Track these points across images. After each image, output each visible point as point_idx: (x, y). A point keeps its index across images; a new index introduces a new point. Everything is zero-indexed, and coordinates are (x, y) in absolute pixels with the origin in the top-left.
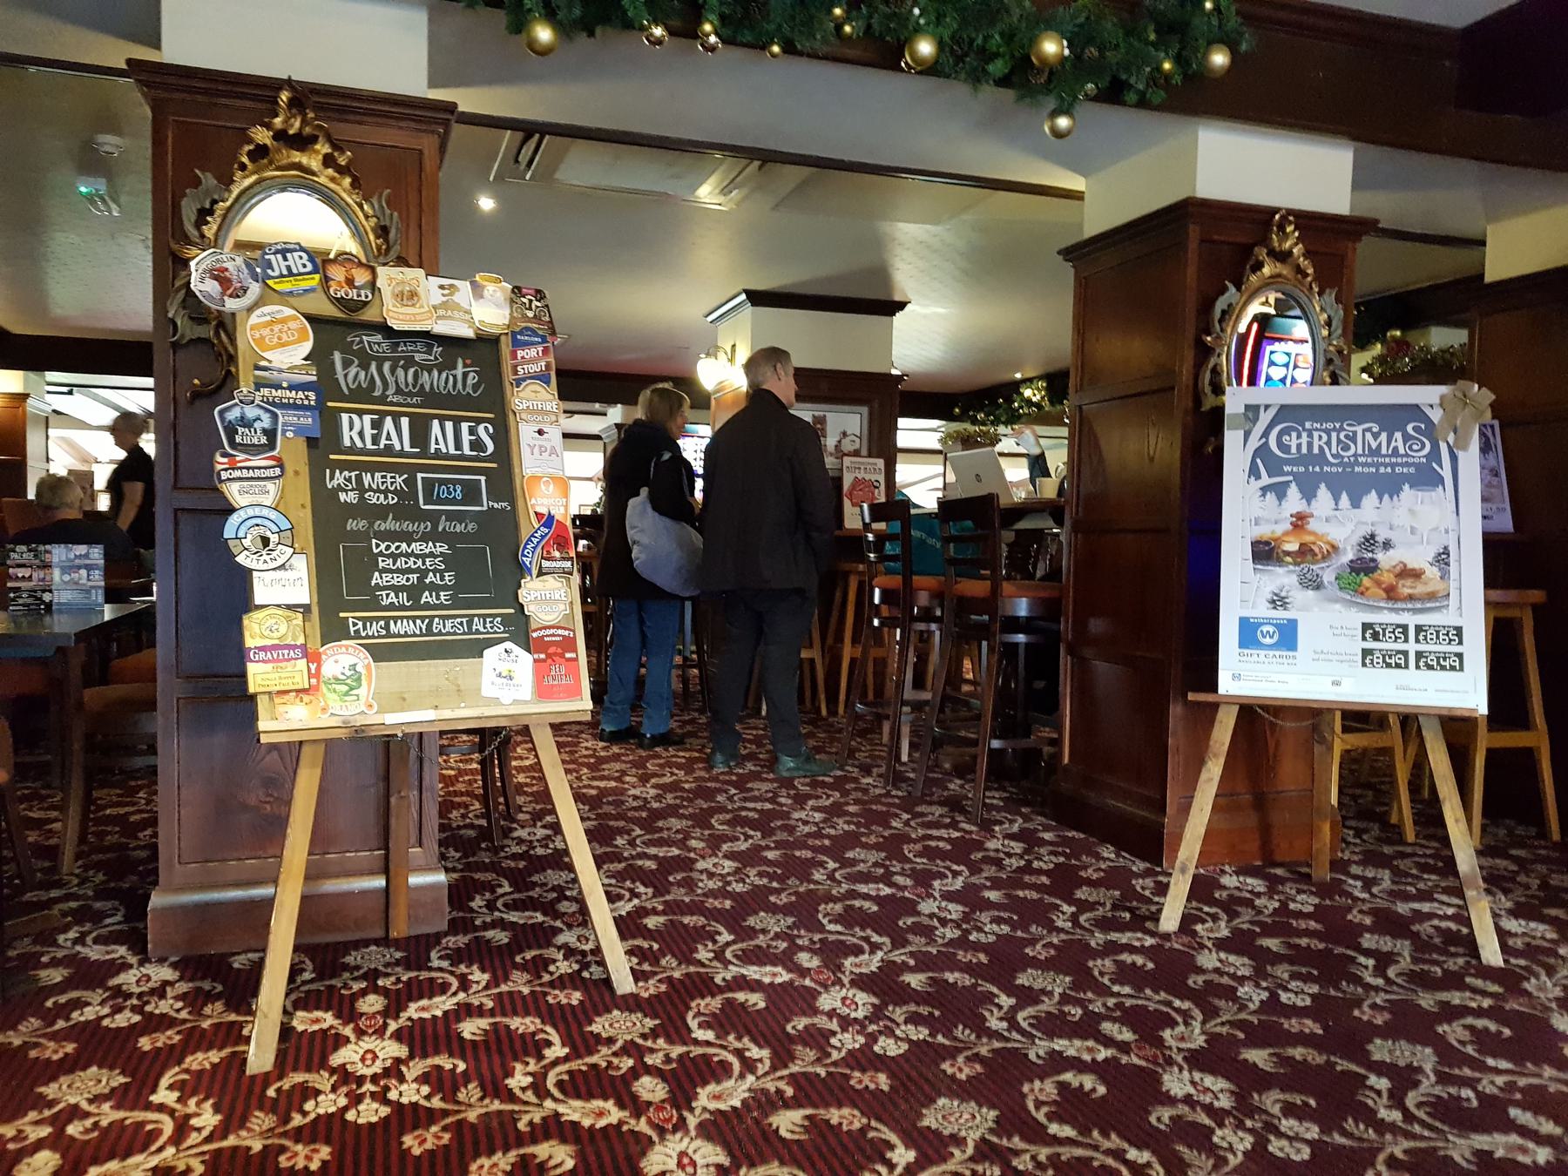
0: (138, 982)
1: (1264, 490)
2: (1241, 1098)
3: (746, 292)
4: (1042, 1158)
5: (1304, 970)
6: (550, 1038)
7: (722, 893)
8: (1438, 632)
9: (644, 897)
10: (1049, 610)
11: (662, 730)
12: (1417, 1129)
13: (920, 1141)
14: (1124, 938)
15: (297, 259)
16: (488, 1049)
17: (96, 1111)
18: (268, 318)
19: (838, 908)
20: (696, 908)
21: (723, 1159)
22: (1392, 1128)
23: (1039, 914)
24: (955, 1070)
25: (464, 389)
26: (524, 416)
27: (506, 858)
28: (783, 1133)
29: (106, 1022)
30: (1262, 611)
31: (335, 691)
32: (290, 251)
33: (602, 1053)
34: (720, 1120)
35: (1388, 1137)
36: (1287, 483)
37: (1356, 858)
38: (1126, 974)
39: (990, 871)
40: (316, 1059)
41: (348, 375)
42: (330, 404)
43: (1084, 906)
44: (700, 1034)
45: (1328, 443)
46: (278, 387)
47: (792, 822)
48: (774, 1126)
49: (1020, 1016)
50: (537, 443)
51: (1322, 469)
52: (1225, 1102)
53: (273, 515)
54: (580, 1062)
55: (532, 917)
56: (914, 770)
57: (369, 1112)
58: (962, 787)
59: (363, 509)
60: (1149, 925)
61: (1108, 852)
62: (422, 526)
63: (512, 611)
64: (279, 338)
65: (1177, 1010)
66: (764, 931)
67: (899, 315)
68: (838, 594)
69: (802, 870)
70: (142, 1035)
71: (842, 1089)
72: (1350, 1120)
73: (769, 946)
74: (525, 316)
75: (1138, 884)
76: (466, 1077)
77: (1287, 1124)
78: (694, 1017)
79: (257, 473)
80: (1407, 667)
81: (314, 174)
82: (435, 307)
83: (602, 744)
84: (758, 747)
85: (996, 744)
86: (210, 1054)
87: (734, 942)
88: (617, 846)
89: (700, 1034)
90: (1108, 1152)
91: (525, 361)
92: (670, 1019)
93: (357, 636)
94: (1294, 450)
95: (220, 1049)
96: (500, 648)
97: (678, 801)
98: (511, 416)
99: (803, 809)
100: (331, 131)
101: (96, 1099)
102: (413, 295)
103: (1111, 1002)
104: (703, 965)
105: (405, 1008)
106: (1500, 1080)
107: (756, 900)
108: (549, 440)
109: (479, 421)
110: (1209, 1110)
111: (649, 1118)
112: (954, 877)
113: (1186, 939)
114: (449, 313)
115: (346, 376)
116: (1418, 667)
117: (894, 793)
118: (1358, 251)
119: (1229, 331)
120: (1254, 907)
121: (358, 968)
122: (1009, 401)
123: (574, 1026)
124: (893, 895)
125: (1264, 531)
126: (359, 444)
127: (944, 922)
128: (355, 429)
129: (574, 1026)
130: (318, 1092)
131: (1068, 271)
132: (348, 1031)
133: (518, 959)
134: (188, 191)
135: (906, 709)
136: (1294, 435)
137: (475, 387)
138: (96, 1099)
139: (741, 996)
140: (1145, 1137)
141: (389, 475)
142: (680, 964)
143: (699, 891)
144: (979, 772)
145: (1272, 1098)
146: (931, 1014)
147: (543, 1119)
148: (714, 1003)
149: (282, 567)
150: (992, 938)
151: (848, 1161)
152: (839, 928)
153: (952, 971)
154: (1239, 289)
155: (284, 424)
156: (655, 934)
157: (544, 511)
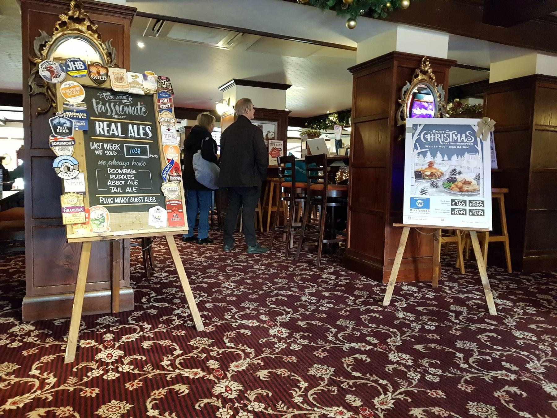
0: (19, 331)
1: (419, 154)
2: (415, 361)
3: (234, 79)
4: (351, 384)
5: (432, 318)
6: (175, 347)
7: (232, 295)
8: (476, 202)
9: (204, 297)
10: (344, 195)
11: (205, 237)
12: (473, 370)
13: (309, 379)
14: (372, 308)
15: (79, 64)
16: (153, 352)
17: (9, 378)
18: (68, 86)
19: (273, 299)
20: (223, 300)
21: (241, 388)
22: (465, 370)
23: (342, 300)
24: (318, 354)
25: (141, 113)
26: (162, 123)
27: (152, 284)
28: (261, 378)
29: (9, 346)
30: (418, 195)
31: (95, 223)
32: (76, 61)
33: (194, 352)
34: (239, 374)
35: (464, 373)
36: (427, 152)
37: (446, 279)
38: (373, 320)
39: (324, 285)
40: (90, 357)
41: (98, 108)
42: (91, 118)
43: (357, 297)
44: (229, 345)
45: (440, 138)
46: (72, 111)
47: (254, 269)
48: (258, 376)
49: (339, 335)
50: (168, 133)
51: (438, 146)
52: (410, 363)
53: (71, 159)
54: (187, 355)
55: (164, 305)
56: (295, 251)
57: (112, 376)
58: (312, 256)
59: (104, 157)
60: (379, 303)
61: (363, 278)
62: (126, 163)
63: (159, 194)
64: (73, 93)
65: (391, 332)
66: (248, 308)
67: (288, 90)
68: (267, 189)
69: (260, 286)
70: (23, 350)
71: (280, 362)
72: (451, 368)
73: (250, 313)
74: (162, 87)
75: (375, 289)
76: (146, 362)
77: (431, 370)
78: (226, 339)
79: (65, 143)
80: (466, 215)
81: (84, 33)
82: (129, 83)
83: (183, 242)
84: (240, 243)
85: (325, 241)
86: (50, 356)
87: (238, 312)
88: (192, 279)
89: (229, 345)
90: (373, 381)
91: (163, 103)
92: (218, 339)
93: (103, 203)
94: (429, 140)
95: (54, 355)
96: (155, 208)
97: (213, 263)
98: (158, 124)
99: (257, 265)
100: (90, 17)
101: (8, 374)
102: (122, 78)
103: (369, 330)
104: (228, 320)
105: (121, 338)
106: (498, 353)
107: (244, 297)
108: (172, 132)
109: (146, 125)
110: (405, 366)
111: (213, 374)
112: (312, 288)
113: (392, 308)
114: (135, 85)
115: (97, 108)
116: (469, 215)
117: (289, 259)
118: (450, 73)
119: (407, 98)
120: (414, 297)
121: (102, 324)
122: (325, 121)
123: (184, 343)
124: (292, 294)
125: (419, 168)
126: (102, 133)
127: (310, 303)
128: (101, 127)
129: (184, 343)
130: (92, 369)
131: (351, 76)
132: (101, 347)
133: (161, 320)
134: (36, 38)
135: (293, 229)
136: (429, 135)
137: (145, 113)
138: (8, 374)
139: (242, 331)
140: (384, 376)
141: (113, 145)
142: (219, 320)
143: (224, 294)
144: (319, 251)
145: (425, 361)
146: (309, 335)
147: (176, 376)
148: (233, 334)
149: (75, 178)
150: (327, 309)
151: (285, 387)
152: (274, 306)
153: (315, 320)
154: (410, 84)
155: (75, 125)
156: (209, 310)
157: (170, 158)
